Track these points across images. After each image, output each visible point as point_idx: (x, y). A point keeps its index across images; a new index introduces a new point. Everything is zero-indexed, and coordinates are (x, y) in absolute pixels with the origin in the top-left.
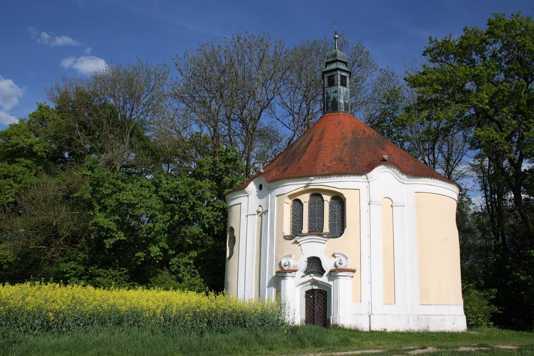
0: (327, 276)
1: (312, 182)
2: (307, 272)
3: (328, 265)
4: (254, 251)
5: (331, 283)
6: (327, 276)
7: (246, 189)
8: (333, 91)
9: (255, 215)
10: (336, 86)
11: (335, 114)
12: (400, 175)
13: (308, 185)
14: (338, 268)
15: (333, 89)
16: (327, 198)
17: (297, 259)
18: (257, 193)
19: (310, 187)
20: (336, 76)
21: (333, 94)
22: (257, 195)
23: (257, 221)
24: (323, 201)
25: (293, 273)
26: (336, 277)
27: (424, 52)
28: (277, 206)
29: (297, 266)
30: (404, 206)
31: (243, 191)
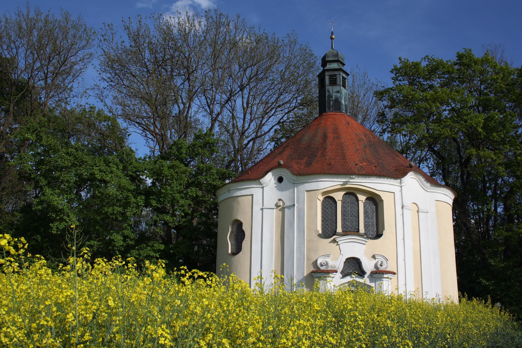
0: (368, 277)
1: (350, 181)
2: (345, 274)
3: (368, 266)
4: (273, 248)
5: (373, 285)
6: (368, 277)
7: (262, 180)
8: (335, 91)
9: (274, 209)
10: (338, 86)
11: (339, 114)
12: (425, 183)
13: (345, 183)
14: (380, 269)
15: (336, 88)
16: (362, 198)
17: (336, 259)
18: (276, 185)
19: (347, 186)
20: (338, 76)
21: (335, 94)
22: (276, 187)
23: (276, 216)
24: (357, 200)
25: (335, 273)
26: (380, 279)
27: (392, 70)
28: (308, 202)
29: (335, 267)
30: (428, 212)
31: (257, 181)
